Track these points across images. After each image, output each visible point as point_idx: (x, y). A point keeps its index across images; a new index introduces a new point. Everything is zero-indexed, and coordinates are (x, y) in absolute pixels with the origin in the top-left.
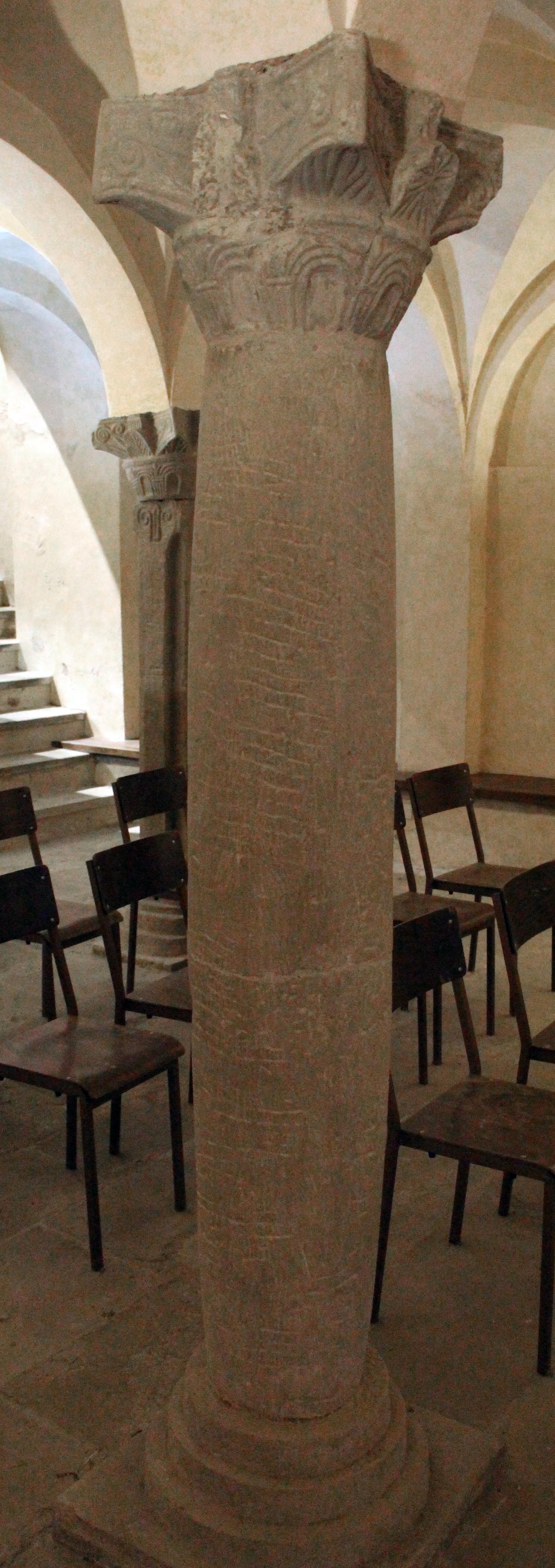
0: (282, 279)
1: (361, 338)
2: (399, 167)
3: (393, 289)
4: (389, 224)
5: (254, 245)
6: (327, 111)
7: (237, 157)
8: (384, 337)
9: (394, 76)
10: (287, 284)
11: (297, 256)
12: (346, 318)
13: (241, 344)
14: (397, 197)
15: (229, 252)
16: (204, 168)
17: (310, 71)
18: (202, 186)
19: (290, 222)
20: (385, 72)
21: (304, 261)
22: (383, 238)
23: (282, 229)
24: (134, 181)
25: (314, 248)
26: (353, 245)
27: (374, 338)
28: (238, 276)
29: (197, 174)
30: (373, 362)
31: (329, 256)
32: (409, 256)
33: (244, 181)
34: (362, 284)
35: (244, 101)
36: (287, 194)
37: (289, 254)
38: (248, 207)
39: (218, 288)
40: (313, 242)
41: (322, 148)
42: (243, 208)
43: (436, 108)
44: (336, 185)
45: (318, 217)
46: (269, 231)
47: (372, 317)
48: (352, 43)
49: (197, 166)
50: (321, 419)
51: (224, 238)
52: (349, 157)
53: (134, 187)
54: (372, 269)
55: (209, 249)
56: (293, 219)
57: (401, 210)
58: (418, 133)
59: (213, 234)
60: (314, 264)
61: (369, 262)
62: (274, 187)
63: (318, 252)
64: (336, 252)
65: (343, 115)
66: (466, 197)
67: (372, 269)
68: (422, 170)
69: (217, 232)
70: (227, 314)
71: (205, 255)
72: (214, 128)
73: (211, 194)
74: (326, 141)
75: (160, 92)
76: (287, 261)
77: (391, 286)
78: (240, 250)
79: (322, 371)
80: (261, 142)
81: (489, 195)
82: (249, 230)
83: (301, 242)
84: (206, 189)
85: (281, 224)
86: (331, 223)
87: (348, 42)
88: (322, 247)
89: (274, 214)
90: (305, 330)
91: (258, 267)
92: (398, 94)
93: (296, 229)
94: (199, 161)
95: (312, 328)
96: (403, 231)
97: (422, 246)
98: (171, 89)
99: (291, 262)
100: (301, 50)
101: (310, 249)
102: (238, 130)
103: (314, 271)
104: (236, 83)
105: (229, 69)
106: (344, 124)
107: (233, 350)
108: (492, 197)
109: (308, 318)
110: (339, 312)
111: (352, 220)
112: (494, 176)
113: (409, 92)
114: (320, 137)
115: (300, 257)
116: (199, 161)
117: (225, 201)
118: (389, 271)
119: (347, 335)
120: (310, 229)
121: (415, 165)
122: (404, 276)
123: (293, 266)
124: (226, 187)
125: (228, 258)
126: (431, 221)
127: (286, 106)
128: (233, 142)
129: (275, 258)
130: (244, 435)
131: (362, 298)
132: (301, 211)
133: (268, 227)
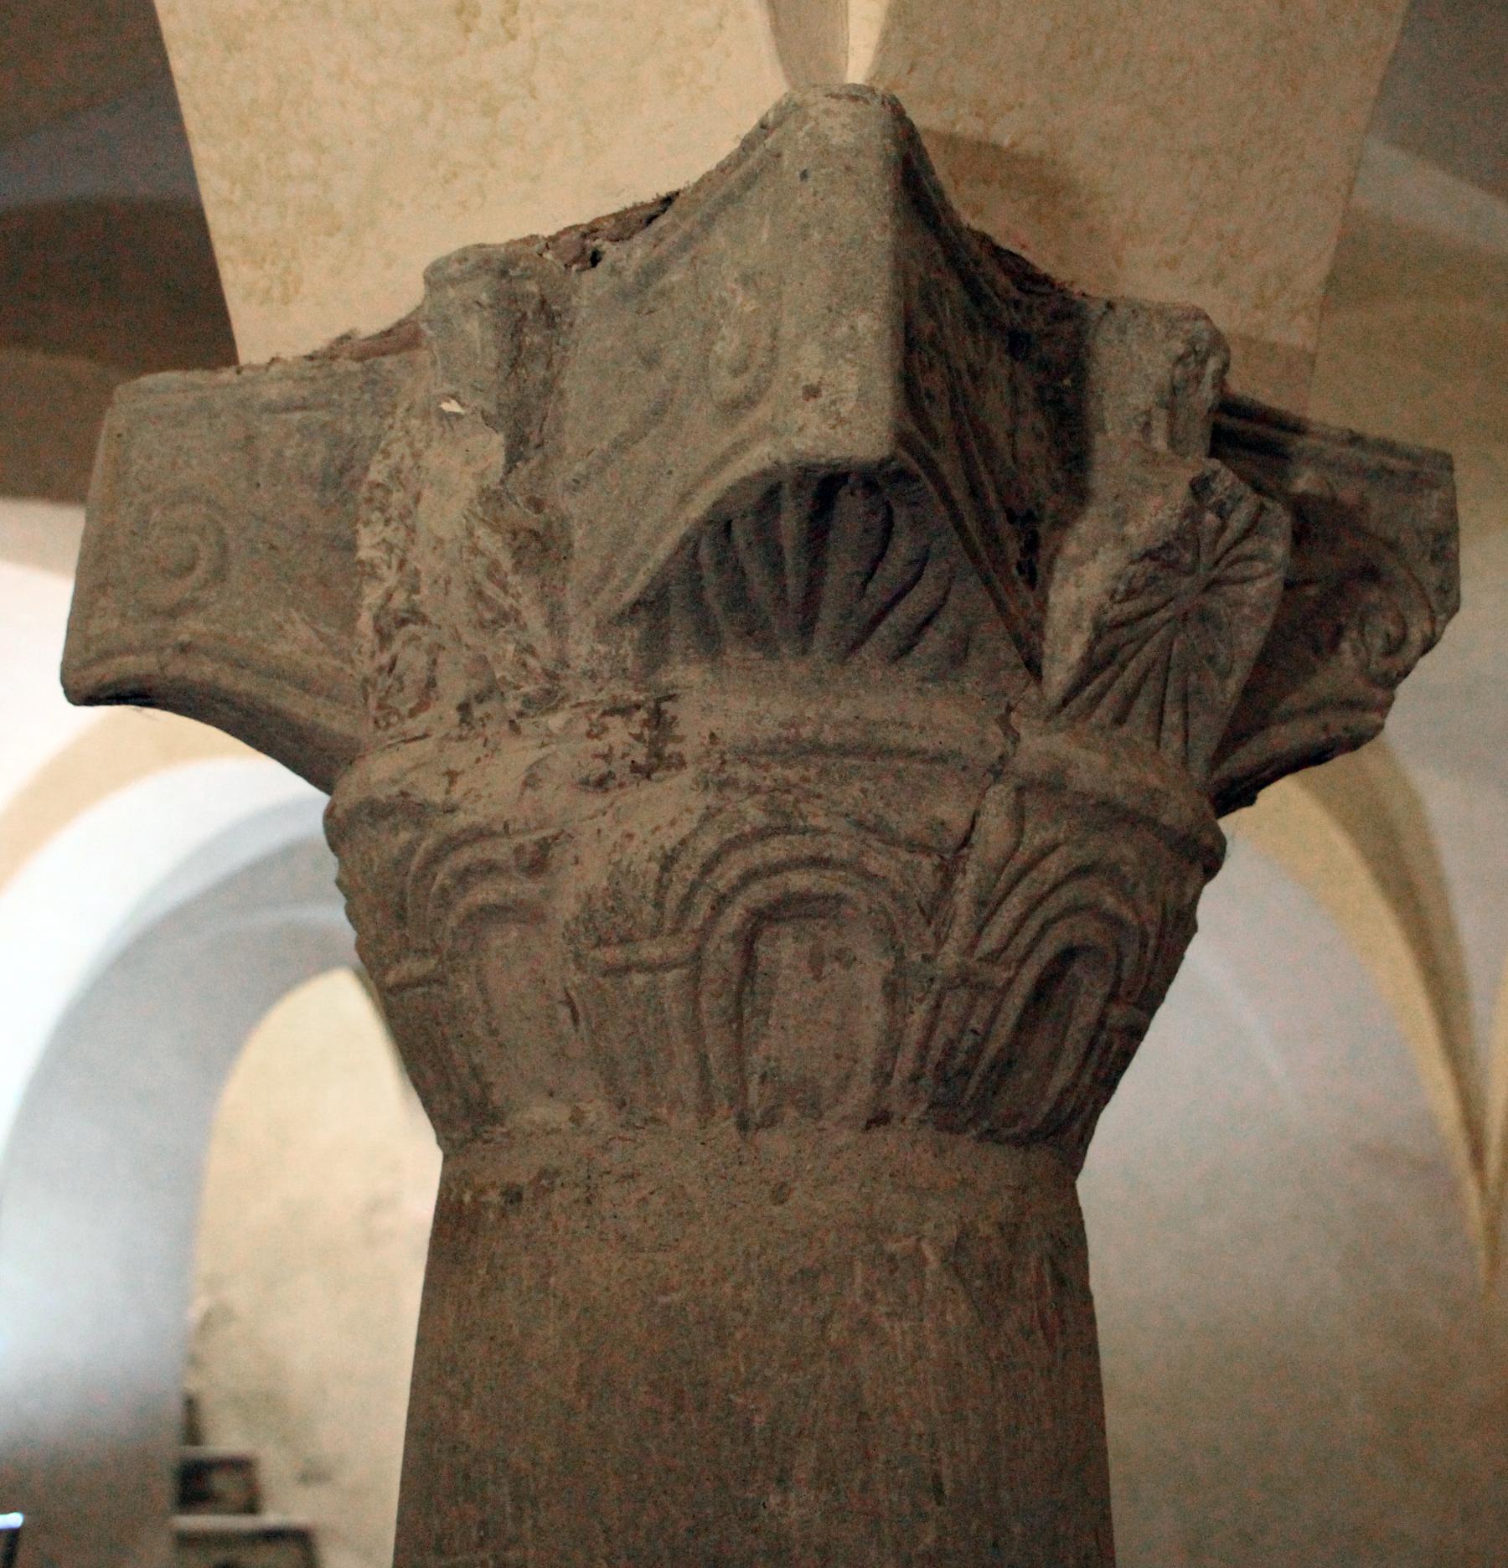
0: (651, 951)
1: (965, 1145)
2: (1072, 549)
3: (1076, 968)
4: (1039, 746)
5: (550, 832)
6: (761, 358)
7: (481, 531)
8: (1066, 1133)
9: (1045, 264)
10: (665, 966)
11: (696, 866)
12: (896, 1082)
13: (523, 1180)
14: (1065, 653)
15: (466, 856)
16: (391, 578)
17: (719, 238)
18: (384, 638)
19: (670, 748)
20: (1007, 245)
21: (721, 885)
22: (1020, 790)
23: (643, 772)
24: (191, 627)
25: (762, 835)
26: (908, 823)
27: (1023, 1142)
28: (503, 939)
29: (372, 595)
30: (1011, 1233)
31: (818, 862)
32: (1125, 850)
33: (505, 617)
34: (950, 957)
35: (516, 359)
36: (655, 651)
37: (668, 861)
38: (528, 701)
39: (441, 981)
40: (754, 814)
41: (746, 482)
42: (514, 705)
43: (1194, 355)
44: (828, 617)
45: (769, 729)
46: (602, 783)
47: (1005, 1065)
48: (841, 128)
49: (370, 572)
50: (806, 1460)
51: (451, 810)
52: (851, 508)
53: (184, 649)
54: (988, 907)
55: (410, 850)
56: (681, 739)
57: (1090, 690)
58: (1135, 435)
59: (418, 796)
60: (758, 894)
61: (967, 882)
62: (609, 626)
63: (776, 850)
64: (842, 850)
65: (809, 362)
66: (1334, 646)
67: (988, 907)
68: (1149, 555)
69: (433, 791)
70: (476, 1072)
71: (399, 864)
72: (419, 445)
73: (414, 661)
74: (759, 457)
75: (288, 354)
76: (662, 886)
77: (1068, 955)
78: (501, 851)
79: (808, 1277)
80: (577, 485)
81: (1416, 636)
82: (531, 781)
83: (708, 816)
84: (396, 646)
85: (640, 754)
86: (818, 748)
87: (828, 122)
88: (788, 830)
89: (616, 722)
90: (743, 1125)
91: (566, 907)
92: (1057, 316)
93: (690, 772)
94: (378, 555)
95: (771, 1120)
96: (1090, 762)
97: (1179, 810)
98: (318, 341)
99: (678, 890)
100: (694, 178)
101: (740, 842)
102: (493, 446)
103: (763, 918)
104: (484, 298)
105: (462, 257)
106: (812, 392)
107: (494, 1197)
108: (1428, 645)
109: (754, 1087)
110: (868, 1062)
111: (896, 737)
112: (1431, 576)
113: (1096, 309)
114: (739, 448)
115: (707, 869)
116: (378, 555)
117: (455, 686)
118: (1052, 906)
119: (908, 1145)
120: (744, 772)
121: (1123, 540)
122: (1116, 921)
123: (687, 903)
124: (457, 638)
125: (464, 877)
126: (1207, 731)
127: (651, 361)
128: (473, 485)
129: (619, 873)
130: (518, 1519)
131: (953, 1007)
132: (707, 709)
133: (599, 768)
